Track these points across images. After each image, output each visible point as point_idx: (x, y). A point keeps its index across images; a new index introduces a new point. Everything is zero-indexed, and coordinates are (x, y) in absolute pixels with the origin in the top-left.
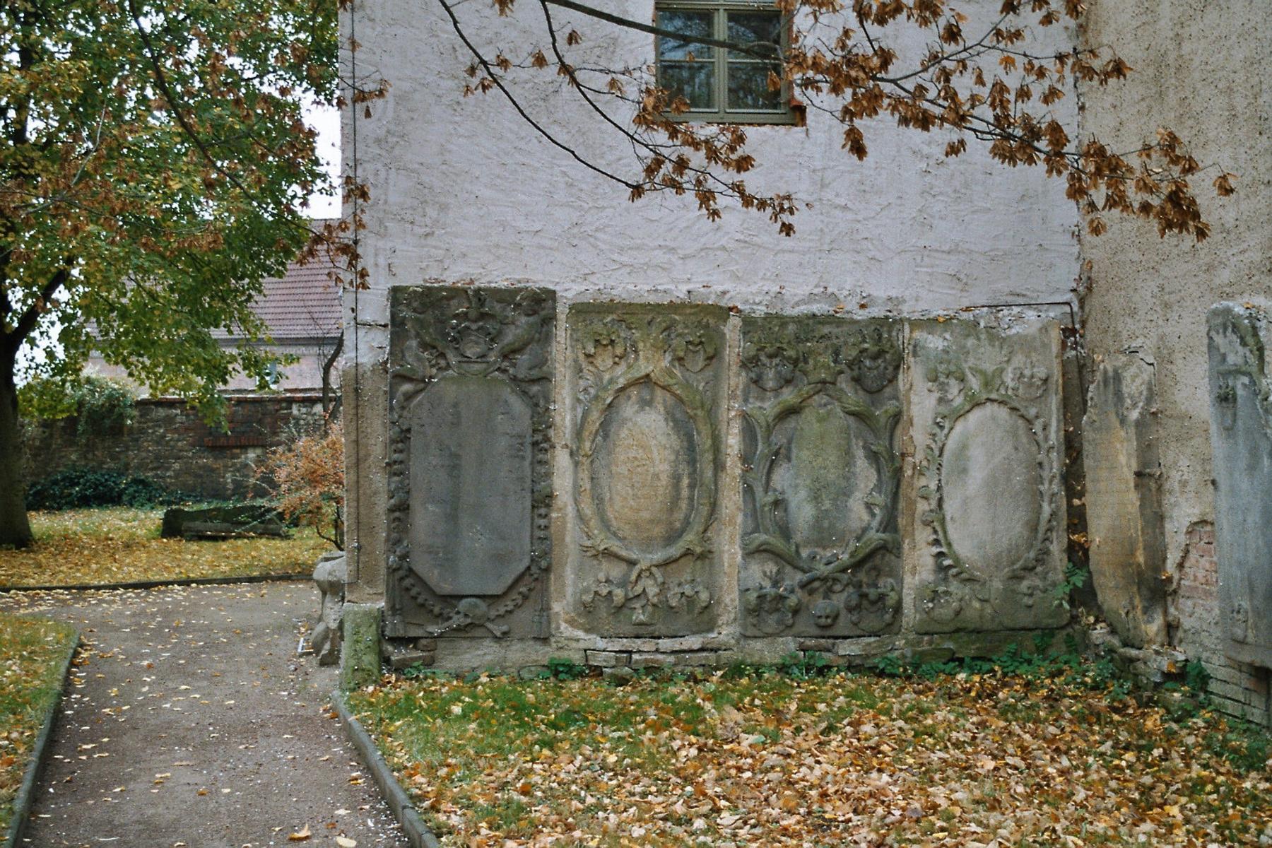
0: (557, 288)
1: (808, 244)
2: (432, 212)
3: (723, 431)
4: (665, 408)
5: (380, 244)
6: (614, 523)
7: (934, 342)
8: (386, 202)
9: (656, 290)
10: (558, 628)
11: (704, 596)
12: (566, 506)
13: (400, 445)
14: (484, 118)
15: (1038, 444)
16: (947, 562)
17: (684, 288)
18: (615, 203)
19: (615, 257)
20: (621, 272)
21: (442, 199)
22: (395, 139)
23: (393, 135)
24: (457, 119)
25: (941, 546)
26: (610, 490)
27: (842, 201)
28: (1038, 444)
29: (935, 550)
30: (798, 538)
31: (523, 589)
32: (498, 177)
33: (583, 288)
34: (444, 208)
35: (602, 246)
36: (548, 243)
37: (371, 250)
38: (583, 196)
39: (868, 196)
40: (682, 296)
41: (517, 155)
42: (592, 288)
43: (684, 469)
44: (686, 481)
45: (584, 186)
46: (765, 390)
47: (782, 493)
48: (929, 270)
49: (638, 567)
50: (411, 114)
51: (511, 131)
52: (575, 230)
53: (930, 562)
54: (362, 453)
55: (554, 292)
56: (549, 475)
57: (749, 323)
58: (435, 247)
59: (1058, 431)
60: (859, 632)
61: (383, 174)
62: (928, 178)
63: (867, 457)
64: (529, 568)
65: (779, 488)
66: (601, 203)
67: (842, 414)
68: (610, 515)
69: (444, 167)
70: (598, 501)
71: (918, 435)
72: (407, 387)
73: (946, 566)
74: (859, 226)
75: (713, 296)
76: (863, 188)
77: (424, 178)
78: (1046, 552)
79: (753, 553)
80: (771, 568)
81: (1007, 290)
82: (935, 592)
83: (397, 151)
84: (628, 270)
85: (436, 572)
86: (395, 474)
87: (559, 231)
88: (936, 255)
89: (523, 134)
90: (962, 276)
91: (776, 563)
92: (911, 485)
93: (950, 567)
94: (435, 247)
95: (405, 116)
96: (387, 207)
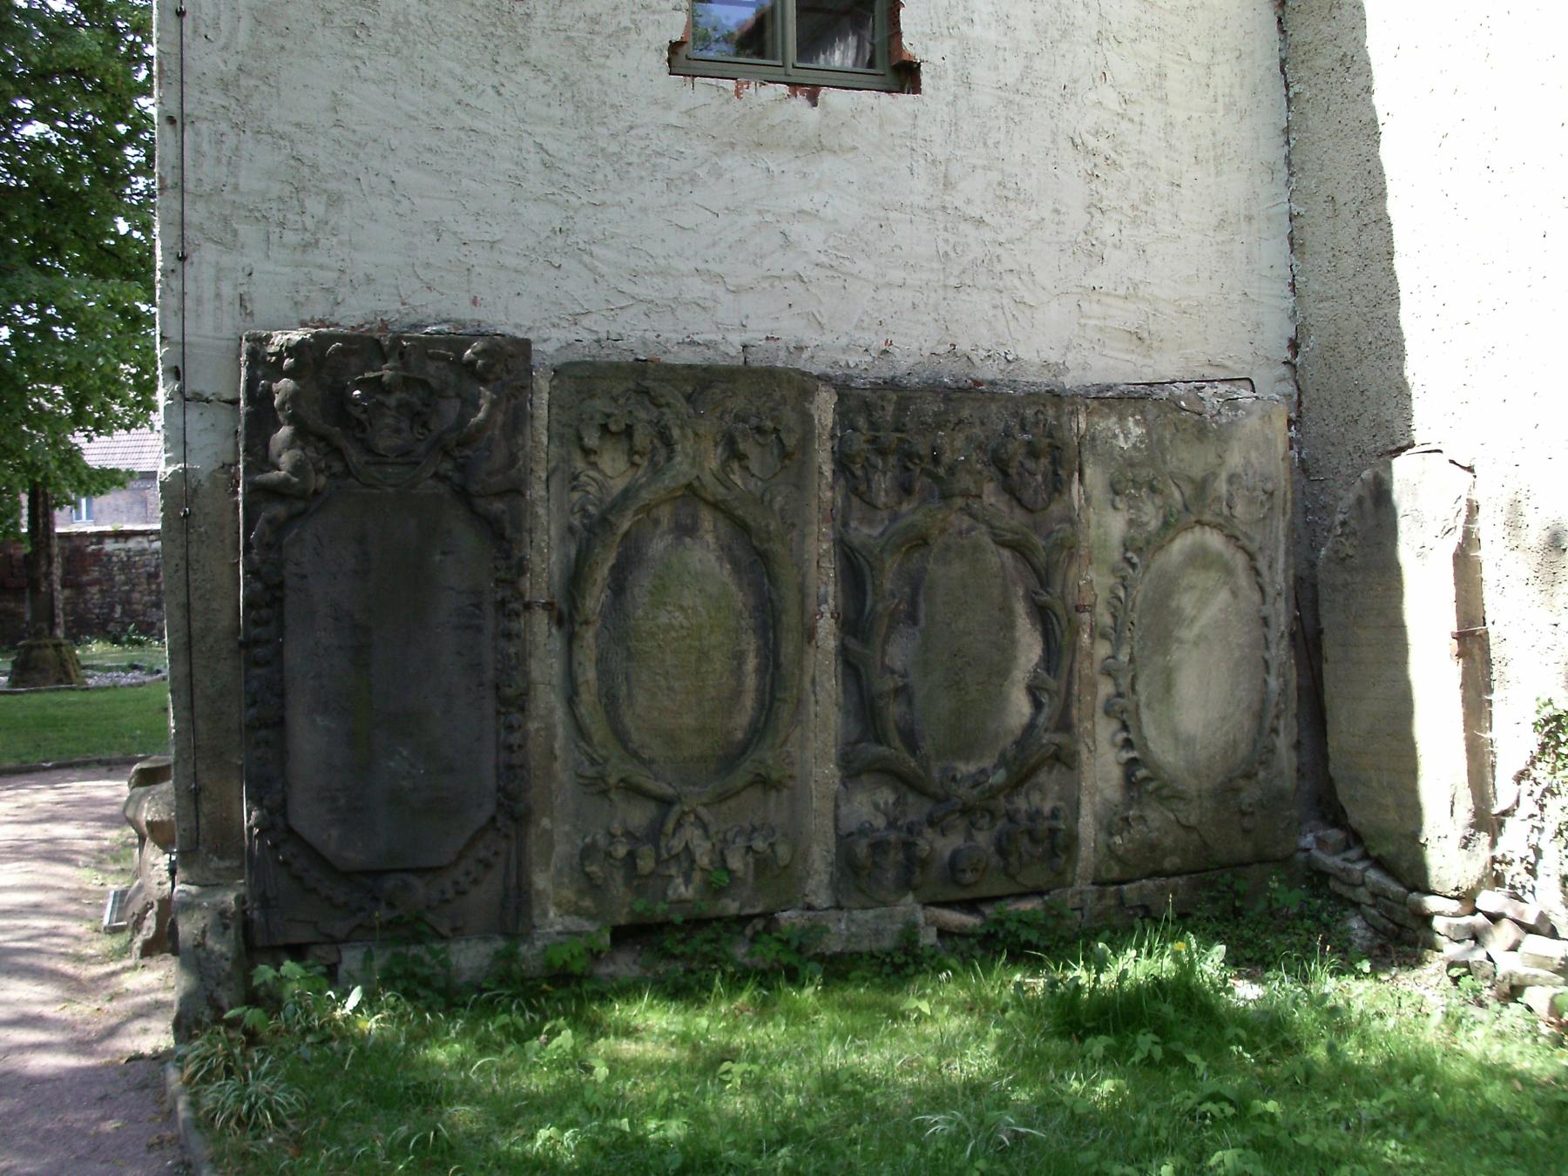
0: (531, 336)
1: (925, 276)
2: (315, 206)
3: (1021, 566)
4: (717, 538)
5: (227, 260)
6: (635, 736)
7: (1128, 434)
8: (236, 188)
9: (693, 343)
10: (545, 914)
11: (783, 851)
12: (552, 711)
13: (264, 612)
14: (406, 52)
15: (1262, 589)
16: (1142, 773)
17: (736, 339)
18: (624, 199)
19: (625, 287)
20: (633, 311)
21: (332, 185)
22: (252, 82)
23: (250, 74)
24: (359, 52)
25: (154, 305)
26: (627, 678)
27: (975, 211)
28: (1262, 589)
29: (1126, 755)
30: (927, 747)
31: (482, 854)
32: (430, 150)
33: (572, 337)
34: (335, 200)
35: (603, 269)
36: (512, 261)
37: (208, 272)
38: (572, 185)
39: (1011, 205)
40: (733, 352)
41: (462, 116)
42: (587, 337)
43: (750, 643)
44: (751, 663)
45: (573, 170)
46: (875, 507)
47: (904, 676)
48: (1100, 323)
49: (677, 809)
50: (281, 41)
51: (451, 73)
52: (559, 241)
53: (1116, 773)
54: (197, 625)
55: (526, 344)
56: (522, 658)
57: (843, 388)
58: (321, 267)
59: (1285, 571)
60: (1016, 889)
61: (231, 140)
62: (1096, 184)
63: (1030, 615)
64: (493, 819)
65: (898, 666)
66: (599, 197)
67: (993, 547)
68: (628, 721)
69: (336, 131)
70: (610, 702)
71: (1094, 581)
72: (279, 510)
73: (1138, 777)
74: (999, 251)
75: (782, 354)
76: (1005, 193)
77: (305, 151)
78: (1272, 750)
79: (852, 770)
80: (886, 796)
81: (1203, 358)
82: (1126, 820)
83: (255, 104)
84: (644, 307)
85: (334, 832)
86: (258, 664)
87: (531, 241)
88: (1109, 300)
89: (472, 81)
90: (1145, 335)
91: (895, 790)
92: (1090, 655)
93: (1147, 779)
94: (321, 267)
95: (269, 43)
96: (237, 198)
